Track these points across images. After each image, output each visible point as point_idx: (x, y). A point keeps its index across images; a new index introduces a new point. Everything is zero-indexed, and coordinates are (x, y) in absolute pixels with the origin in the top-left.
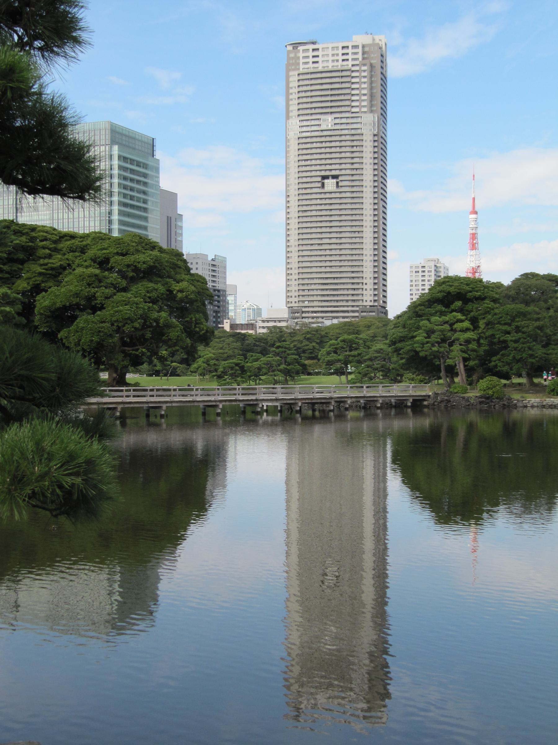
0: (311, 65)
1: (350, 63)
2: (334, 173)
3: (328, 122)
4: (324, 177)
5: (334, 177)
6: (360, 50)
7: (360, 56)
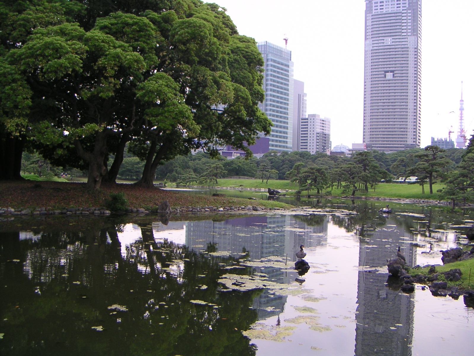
0: (379, 10)
1: (401, 9)
2: (391, 69)
3: (389, 41)
4: (388, 72)
5: (392, 71)
7: (407, 5)
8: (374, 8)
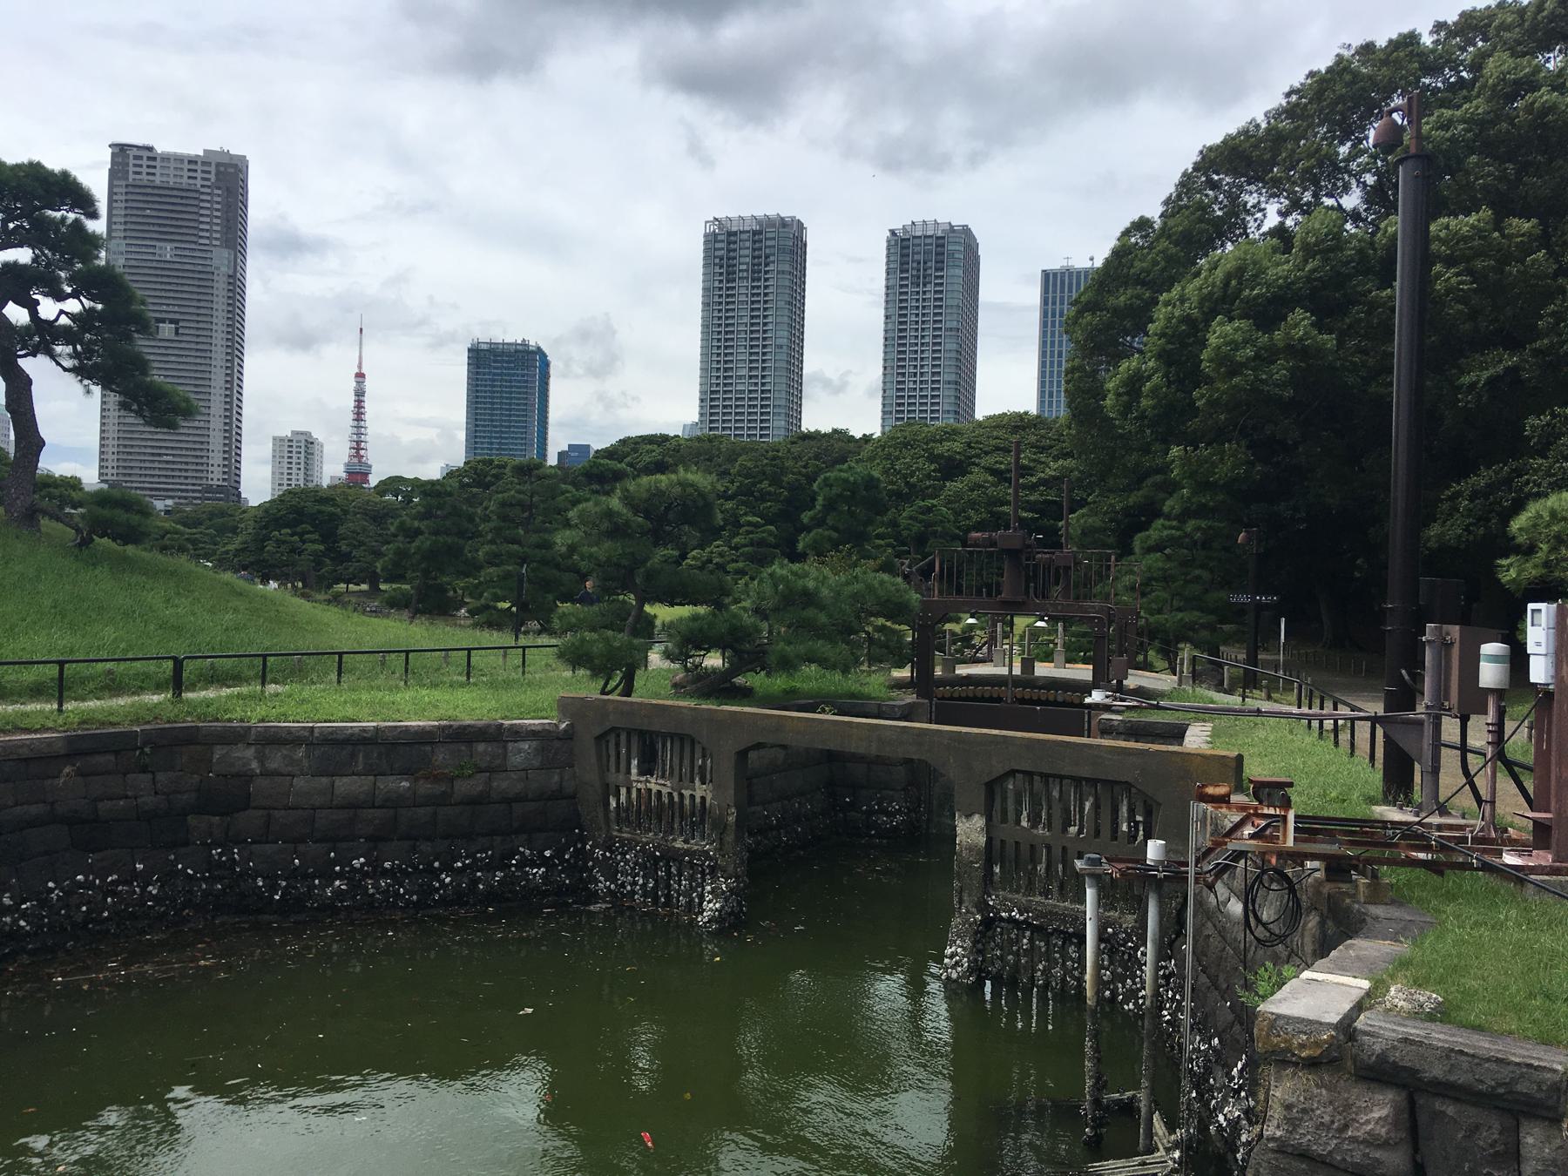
1: (199, 182)
2: (171, 316)
4: (163, 321)
6: (213, 169)
7: (213, 177)
8: (131, 169)
